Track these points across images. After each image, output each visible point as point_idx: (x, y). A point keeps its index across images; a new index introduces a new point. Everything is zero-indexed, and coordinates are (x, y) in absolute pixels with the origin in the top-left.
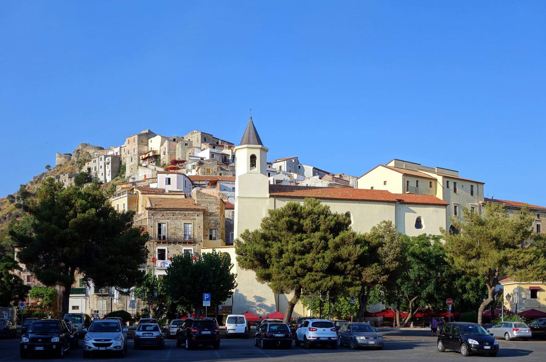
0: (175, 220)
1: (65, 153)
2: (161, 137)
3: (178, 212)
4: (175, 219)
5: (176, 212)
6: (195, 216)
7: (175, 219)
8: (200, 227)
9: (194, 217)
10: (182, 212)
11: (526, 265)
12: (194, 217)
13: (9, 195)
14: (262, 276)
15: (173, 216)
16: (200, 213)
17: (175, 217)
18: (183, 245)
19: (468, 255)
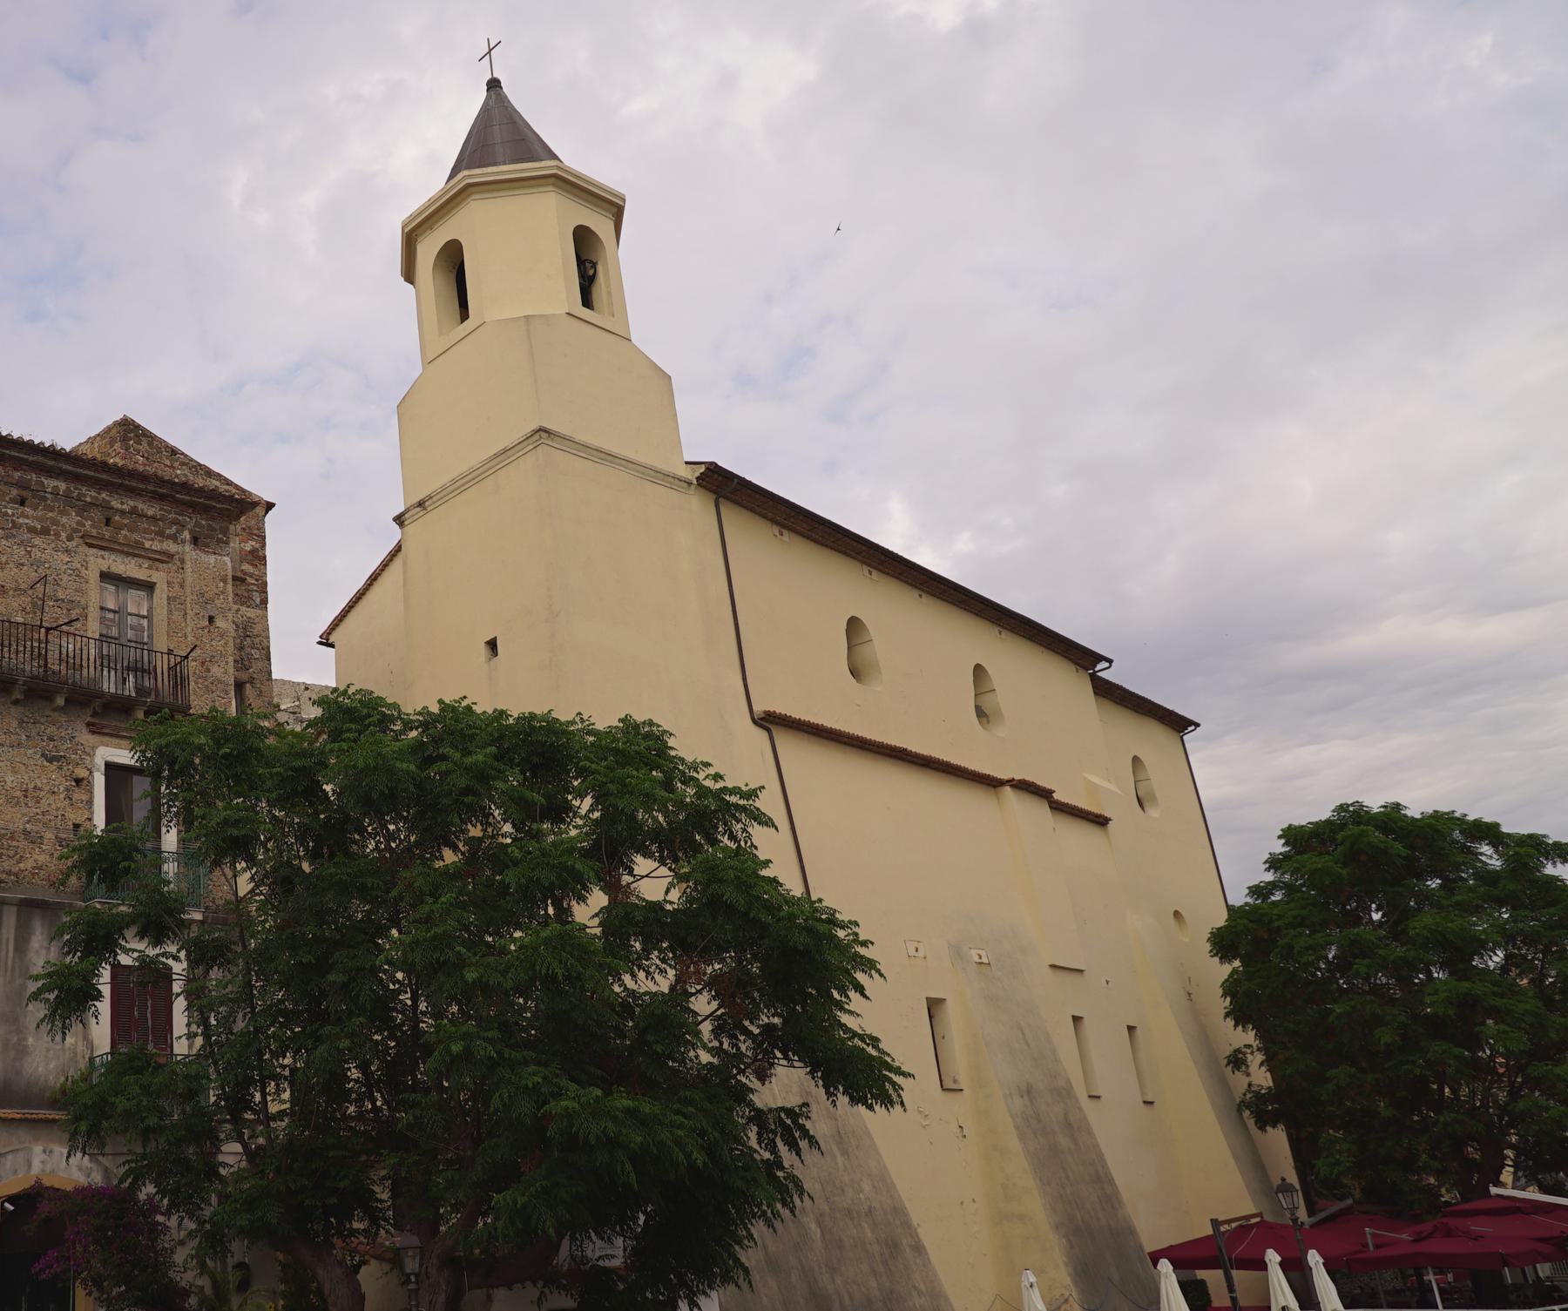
0: (37, 541)
1: (1142, 812)
2: (633, 341)
3: (62, 486)
4: (32, 530)
5: (50, 483)
6: (174, 538)
7: (32, 530)
8: (211, 619)
9: (172, 547)
10: (90, 494)
11: (248, 636)
12: (172, 547)
13: (716, 773)
14: (835, 1098)
15: (22, 503)
16: (211, 528)
17: (29, 516)
18: (95, 729)
19: (861, 1180)
